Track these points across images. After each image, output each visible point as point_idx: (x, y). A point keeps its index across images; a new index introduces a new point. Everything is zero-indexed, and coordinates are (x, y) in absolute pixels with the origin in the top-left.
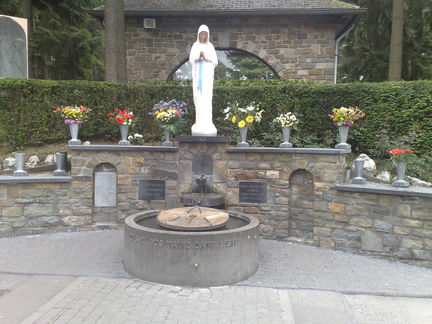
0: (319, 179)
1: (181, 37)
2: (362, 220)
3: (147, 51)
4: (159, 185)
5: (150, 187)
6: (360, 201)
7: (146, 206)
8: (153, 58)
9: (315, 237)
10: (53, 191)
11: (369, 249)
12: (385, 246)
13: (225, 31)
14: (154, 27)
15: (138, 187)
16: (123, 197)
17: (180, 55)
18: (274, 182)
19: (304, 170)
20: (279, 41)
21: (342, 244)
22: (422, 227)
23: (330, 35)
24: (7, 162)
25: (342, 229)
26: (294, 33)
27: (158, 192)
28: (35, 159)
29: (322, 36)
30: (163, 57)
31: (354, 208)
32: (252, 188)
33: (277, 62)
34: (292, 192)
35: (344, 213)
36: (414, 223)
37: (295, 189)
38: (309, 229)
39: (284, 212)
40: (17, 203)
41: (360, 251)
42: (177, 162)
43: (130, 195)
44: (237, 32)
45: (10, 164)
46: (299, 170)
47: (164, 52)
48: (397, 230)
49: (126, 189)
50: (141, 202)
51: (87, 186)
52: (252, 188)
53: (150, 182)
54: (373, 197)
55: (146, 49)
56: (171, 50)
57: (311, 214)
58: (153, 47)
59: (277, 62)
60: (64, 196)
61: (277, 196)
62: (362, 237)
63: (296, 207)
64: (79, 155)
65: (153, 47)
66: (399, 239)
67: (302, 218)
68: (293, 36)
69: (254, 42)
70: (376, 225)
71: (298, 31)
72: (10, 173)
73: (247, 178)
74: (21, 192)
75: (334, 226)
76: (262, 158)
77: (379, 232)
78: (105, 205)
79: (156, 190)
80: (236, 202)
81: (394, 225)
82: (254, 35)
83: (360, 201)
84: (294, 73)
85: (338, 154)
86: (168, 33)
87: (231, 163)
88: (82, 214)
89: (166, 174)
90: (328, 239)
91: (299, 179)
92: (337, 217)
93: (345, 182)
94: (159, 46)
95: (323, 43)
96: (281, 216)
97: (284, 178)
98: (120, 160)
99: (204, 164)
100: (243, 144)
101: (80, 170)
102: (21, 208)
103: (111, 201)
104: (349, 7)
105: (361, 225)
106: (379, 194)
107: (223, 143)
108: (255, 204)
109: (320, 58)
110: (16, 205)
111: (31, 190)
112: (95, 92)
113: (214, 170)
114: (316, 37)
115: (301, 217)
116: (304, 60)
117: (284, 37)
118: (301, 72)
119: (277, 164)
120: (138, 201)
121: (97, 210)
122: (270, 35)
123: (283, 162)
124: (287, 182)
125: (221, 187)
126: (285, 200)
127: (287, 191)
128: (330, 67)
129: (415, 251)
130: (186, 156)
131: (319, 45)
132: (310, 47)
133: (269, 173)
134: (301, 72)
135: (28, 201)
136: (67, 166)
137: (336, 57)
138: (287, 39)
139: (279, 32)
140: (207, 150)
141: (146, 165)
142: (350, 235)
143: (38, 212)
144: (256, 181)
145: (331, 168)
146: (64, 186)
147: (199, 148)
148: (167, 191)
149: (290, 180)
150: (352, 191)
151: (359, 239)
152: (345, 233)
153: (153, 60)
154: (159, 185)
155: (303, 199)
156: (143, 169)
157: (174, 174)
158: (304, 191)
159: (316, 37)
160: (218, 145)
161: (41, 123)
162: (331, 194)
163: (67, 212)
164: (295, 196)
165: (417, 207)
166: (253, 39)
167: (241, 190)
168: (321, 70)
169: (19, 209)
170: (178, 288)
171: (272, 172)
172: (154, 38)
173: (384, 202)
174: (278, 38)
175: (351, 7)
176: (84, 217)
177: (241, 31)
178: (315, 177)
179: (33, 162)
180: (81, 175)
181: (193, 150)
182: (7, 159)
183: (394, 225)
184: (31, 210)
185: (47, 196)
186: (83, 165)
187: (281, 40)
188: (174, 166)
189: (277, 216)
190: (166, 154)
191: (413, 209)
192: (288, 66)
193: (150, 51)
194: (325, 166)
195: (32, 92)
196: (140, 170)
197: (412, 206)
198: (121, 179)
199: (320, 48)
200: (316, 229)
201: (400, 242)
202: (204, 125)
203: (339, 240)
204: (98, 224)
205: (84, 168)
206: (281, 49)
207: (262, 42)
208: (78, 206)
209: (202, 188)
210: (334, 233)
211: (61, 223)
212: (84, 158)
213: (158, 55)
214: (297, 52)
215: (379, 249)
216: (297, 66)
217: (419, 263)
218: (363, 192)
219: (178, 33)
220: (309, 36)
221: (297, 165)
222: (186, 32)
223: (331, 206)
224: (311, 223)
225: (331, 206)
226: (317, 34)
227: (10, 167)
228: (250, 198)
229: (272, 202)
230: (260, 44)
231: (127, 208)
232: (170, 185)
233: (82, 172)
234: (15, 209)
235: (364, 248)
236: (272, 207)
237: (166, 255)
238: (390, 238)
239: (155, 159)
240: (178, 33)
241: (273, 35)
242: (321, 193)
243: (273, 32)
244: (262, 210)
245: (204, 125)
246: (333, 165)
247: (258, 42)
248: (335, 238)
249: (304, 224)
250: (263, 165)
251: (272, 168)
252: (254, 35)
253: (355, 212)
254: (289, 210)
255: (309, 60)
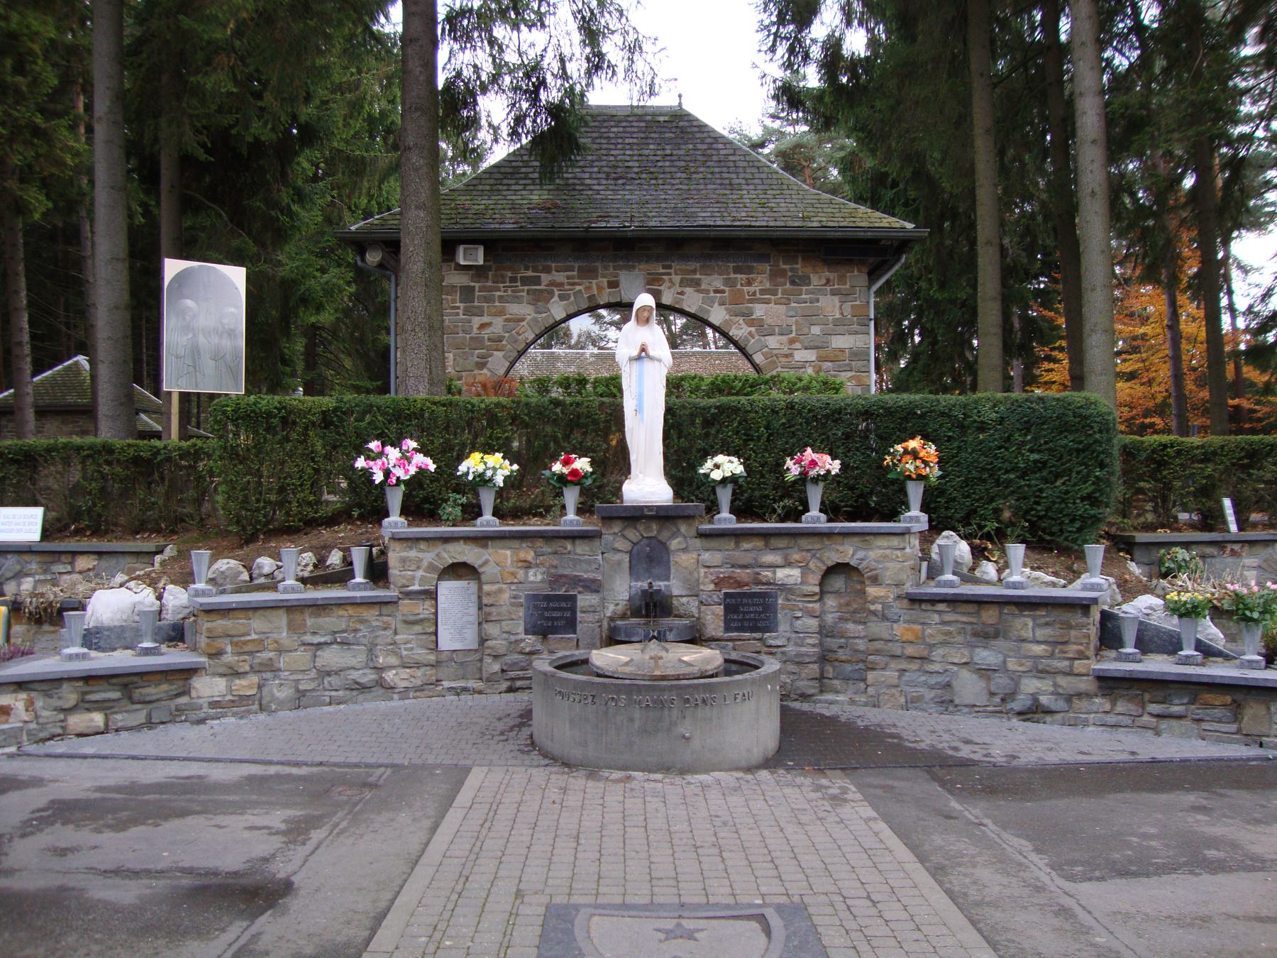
0: (875, 580)
1: (537, 281)
2: (952, 651)
3: (461, 312)
4: (563, 605)
5: (546, 609)
6: (947, 617)
7: (539, 647)
8: (476, 326)
9: (869, 689)
10: (367, 621)
11: (967, 702)
12: (992, 694)
13: (634, 267)
14: (481, 263)
15: (522, 609)
16: (492, 629)
17: (535, 320)
18: (790, 589)
19: (847, 565)
20: (751, 289)
21: (919, 699)
22: (1052, 656)
23: (857, 277)
24: (260, 567)
25: (919, 670)
26: (783, 273)
27: (561, 618)
28: (309, 557)
29: (842, 280)
30: (498, 325)
31: (939, 631)
32: (748, 605)
33: (750, 333)
34: (826, 608)
35: (920, 639)
36: (1038, 649)
37: (831, 602)
38: (856, 676)
39: (810, 647)
40: (304, 644)
41: (951, 708)
42: (600, 557)
43: (506, 625)
44: (662, 271)
45: (266, 570)
46: (838, 564)
47: (501, 313)
48: (1012, 665)
49: (499, 614)
50: (531, 639)
51: (424, 609)
52: (748, 605)
53: (548, 598)
54: (971, 608)
55: (458, 308)
56: (515, 309)
57: (862, 647)
58: (476, 304)
59: (750, 333)
60: (385, 629)
61: (798, 618)
62: (954, 683)
63: (833, 636)
64: (411, 548)
65: (476, 304)
66: (1016, 679)
67: (844, 658)
68: (780, 280)
69: (698, 291)
70: (976, 659)
71: (791, 270)
72: (273, 587)
73: (739, 584)
74: (310, 622)
75: (903, 667)
76: (766, 545)
77: (985, 672)
78: (458, 646)
79: (558, 614)
80: (720, 633)
81: (1006, 656)
82: (698, 276)
83: (947, 617)
84: (786, 356)
85: (904, 533)
86: (509, 274)
87: (706, 556)
88: (418, 665)
89: (576, 581)
90: (894, 691)
91: (838, 583)
92: (910, 650)
93: (918, 585)
94: (488, 300)
95: (844, 295)
96: (806, 655)
97: (811, 581)
98: (487, 557)
99: (651, 558)
100: (725, 519)
101: (413, 578)
102: (310, 653)
103: (470, 641)
104: (894, 225)
105: (951, 660)
106: (980, 602)
107: (688, 518)
108: (754, 635)
109: (840, 325)
110: (302, 648)
111: (327, 619)
112: (409, 417)
113: (673, 571)
114: (828, 282)
115: (842, 654)
116: (805, 330)
117: (761, 282)
118: (801, 355)
119: (796, 556)
120: (523, 636)
121: (443, 657)
122: (732, 276)
123: (808, 551)
124: (817, 589)
125: (692, 606)
126: (813, 623)
127: (817, 606)
128: (860, 344)
129: (1041, 698)
130: (617, 545)
131: (836, 299)
132: (818, 301)
133: (781, 574)
134: (801, 355)
135: (322, 640)
136: (378, 572)
137: (872, 323)
138: (768, 286)
139: (749, 270)
140: (659, 532)
141: (537, 565)
142: (933, 680)
143: (341, 660)
144: (756, 589)
145: (896, 560)
146: (385, 610)
147: (641, 527)
148: (579, 614)
149: (821, 584)
150: (933, 600)
151: (948, 685)
152: (923, 678)
153: (475, 330)
154: (563, 605)
155: (847, 620)
156: (531, 572)
157: (594, 581)
158: (848, 604)
159: (828, 282)
160: (680, 522)
161: (301, 485)
162: (898, 608)
163: (393, 660)
164: (830, 616)
165: (1043, 621)
166: (696, 284)
167: (729, 609)
168: (842, 350)
169: (308, 655)
170: (659, 776)
171: (787, 571)
172: (477, 285)
173: (989, 616)
174: (749, 283)
175: (898, 225)
176: (423, 669)
177: (670, 267)
178: (869, 578)
179: (306, 565)
180: (416, 587)
181: (633, 534)
182: (259, 560)
183: (1006, 656)
184: (331, 657)
185: (356, 631)
186: (418, 568)
187: (756, 288)
188: (594, 566)
189: (799, 655)
190: (578, 542)
191: (1036, 625)
192: (773, 342)
193: (470, 312)
194: (886, 556)
195: (284, 421)
196: (527, 573)
197: (1034, 620)
198: (489, 594)
199: (838, 304)
200: (871, 676)
201: (1017, 684)
202: (647, 484)
203: (913, 691)
204: (446, 684)
205: (420, 573)
206: (757, 305)
207: (716, 291)
208: (412, 649)
209: (652, 607)
210: (904, 678)
211: (380, 683)
212: (421, 555)
213: (486, 319)
214: (791, 313)
215: (982, 700)
216: (792, 341)
217: (1048, 718)
218: (954, 601)
219: (530, 273)
220: (815, 280)
221: (833, 558)
222: (548, 270)
223: (899, 629)
224: (861, 665)
225: (899, 629)
226: (831, 276)
227: (267, 576)
228: (746, 624)
229: (788, 628)
230: (712, 294)
231: (501, 652)
232: (587, 603)
233: (417, 582)
234: (301, 657)
235: (957, 701)
236: (789, 639)
237: (632, 720)
238: (1001, 681)
239: (556, 553)
240: (530, 273)
241: (738, 276)
242: (879, 607)
243: (737, 270)
244: (770, 646)
245: (647, 484)
246: (898, 553)
247: (707, 292)
248: (908, 689)
249: (848, 667)
250: (770, 558)
251: (788, 564)
252: (698, 276)
253: (940, 638)
254: (821, 644)
255: (816, 330)
